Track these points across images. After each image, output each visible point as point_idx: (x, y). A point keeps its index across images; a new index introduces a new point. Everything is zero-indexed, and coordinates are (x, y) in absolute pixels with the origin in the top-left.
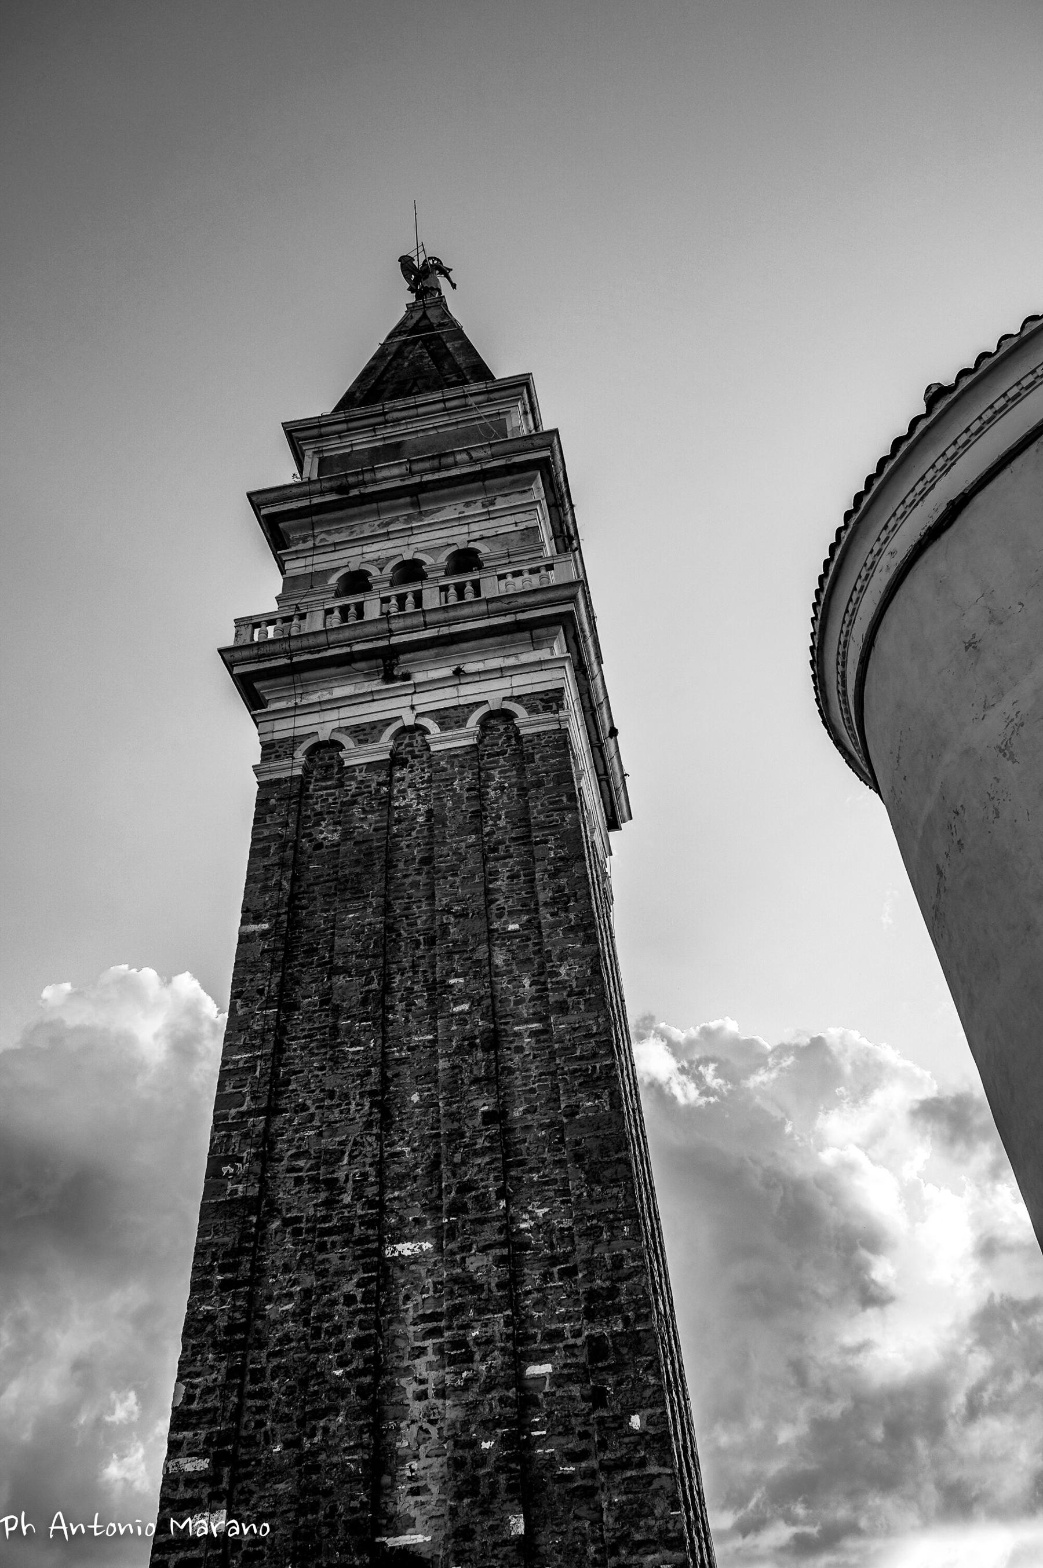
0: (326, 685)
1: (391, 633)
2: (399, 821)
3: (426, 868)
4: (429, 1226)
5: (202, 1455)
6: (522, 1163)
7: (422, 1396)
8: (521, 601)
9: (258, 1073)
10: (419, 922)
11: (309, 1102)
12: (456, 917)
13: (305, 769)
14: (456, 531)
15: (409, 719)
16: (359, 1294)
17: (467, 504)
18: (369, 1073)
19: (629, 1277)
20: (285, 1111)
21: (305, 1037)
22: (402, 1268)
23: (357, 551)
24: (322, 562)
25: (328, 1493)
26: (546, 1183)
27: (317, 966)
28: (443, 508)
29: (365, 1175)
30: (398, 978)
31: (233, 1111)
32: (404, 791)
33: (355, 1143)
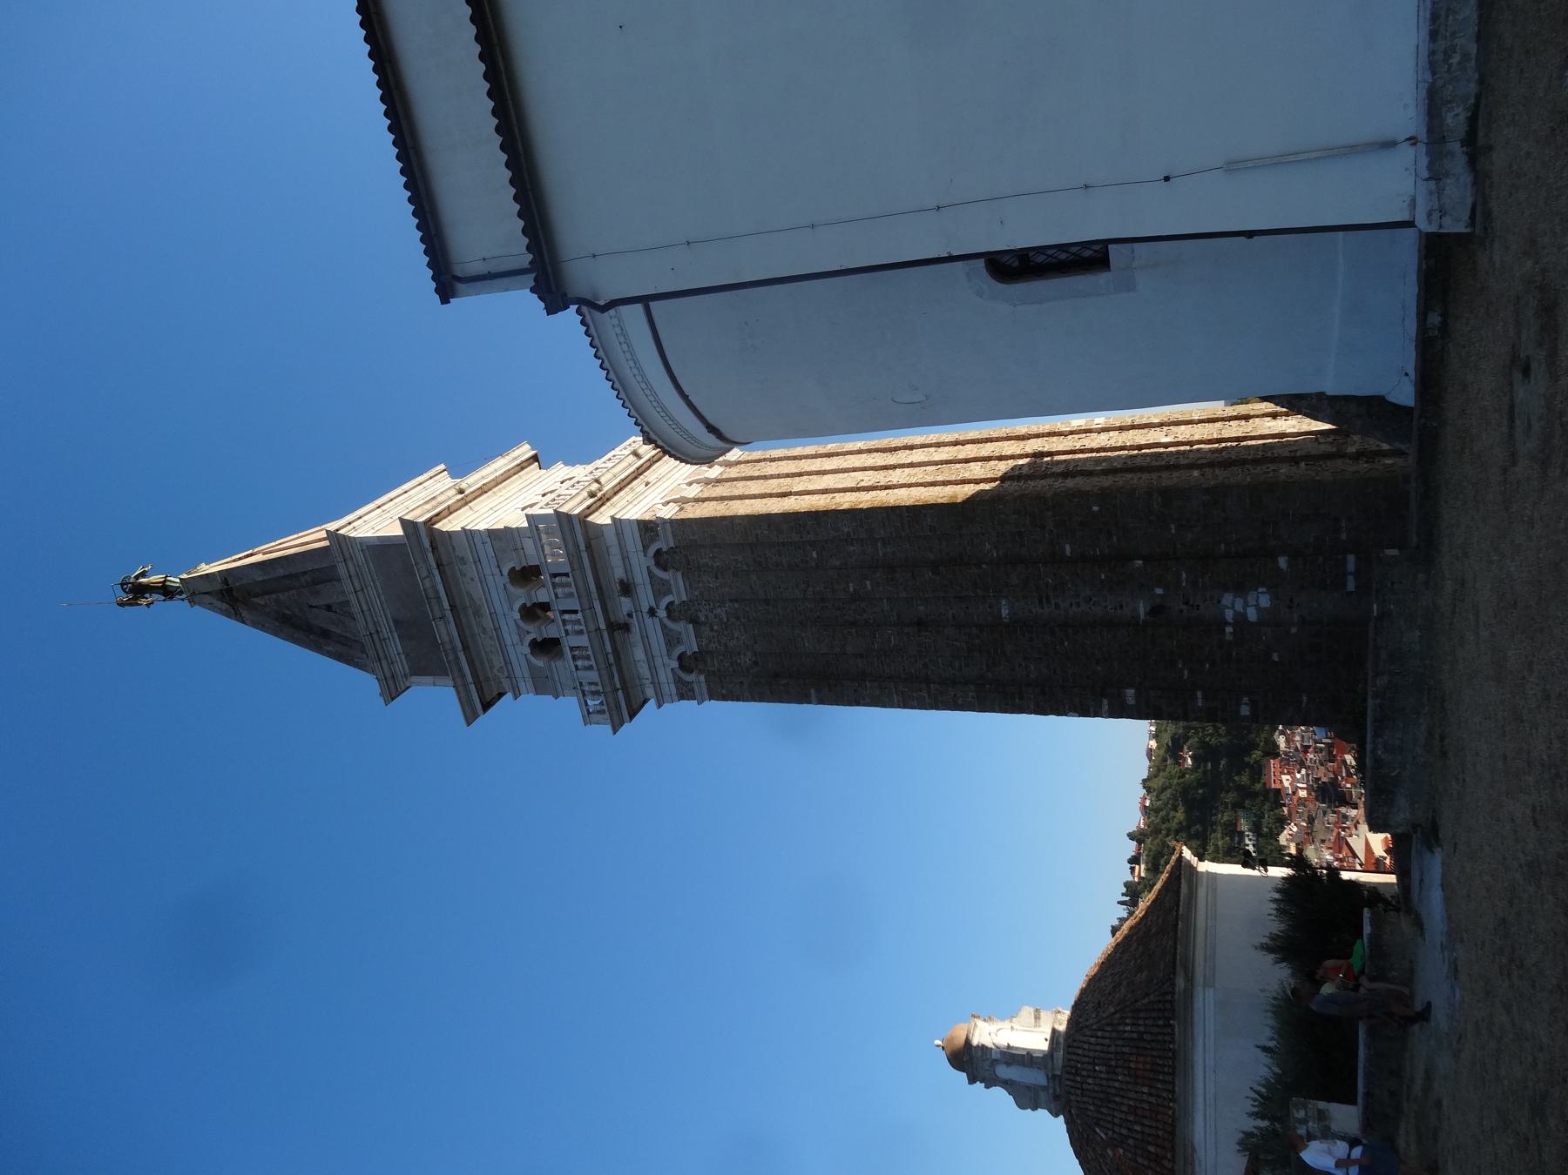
7: (1078, 604)
13: (701, 672)
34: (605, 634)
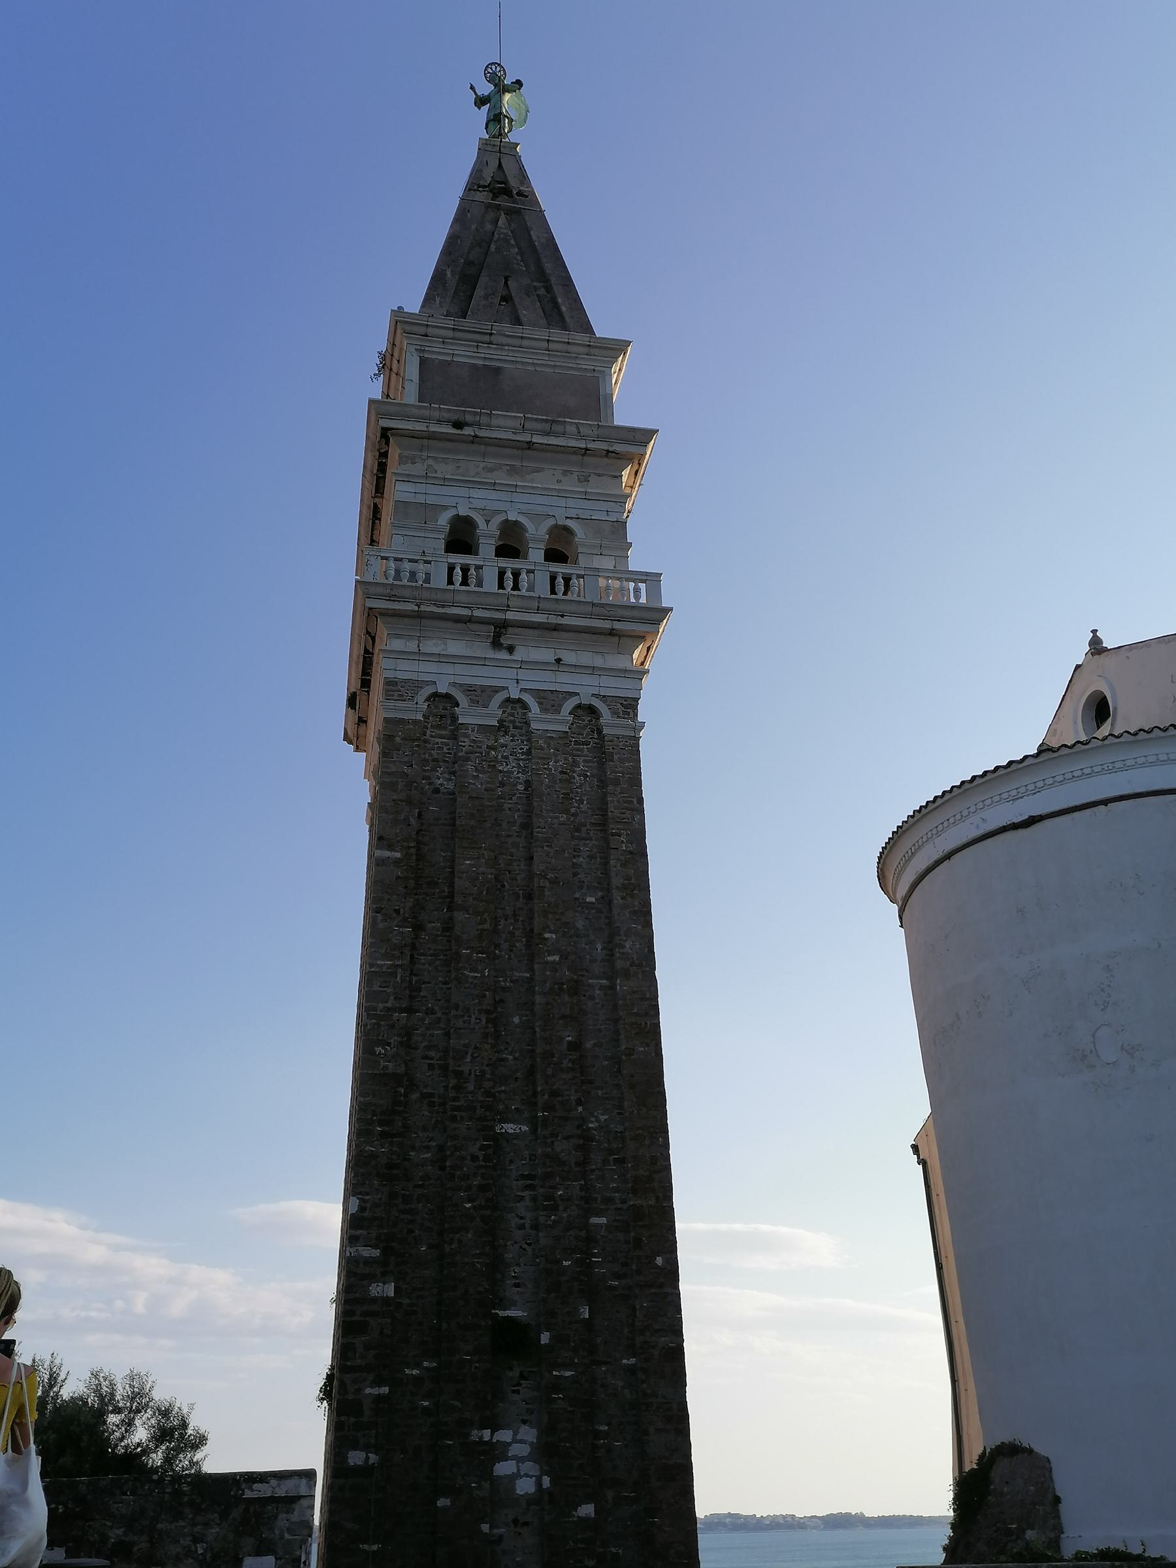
2: (502, 784)
3: (524, 832)
4: (526, 1115)
5: (375, 1247)
6: (591, 1082)
7: (522, 1227)
8: (620, 612)
10: (519, 878)
11: (436, 1008)
12: (551, 883)
16: (481, 1155)
18: (485, 996)
20: (418, 1011)
22: (508, 1141)
23: (463, 492)
24: (434, 494)
26: (607, 1099)
28: (543, 469)
29: (483, 1072)
30: (503, 922)
31: (381, 1006)
32: (506, 757)
33: (476, 1048)
34: (499, 615)
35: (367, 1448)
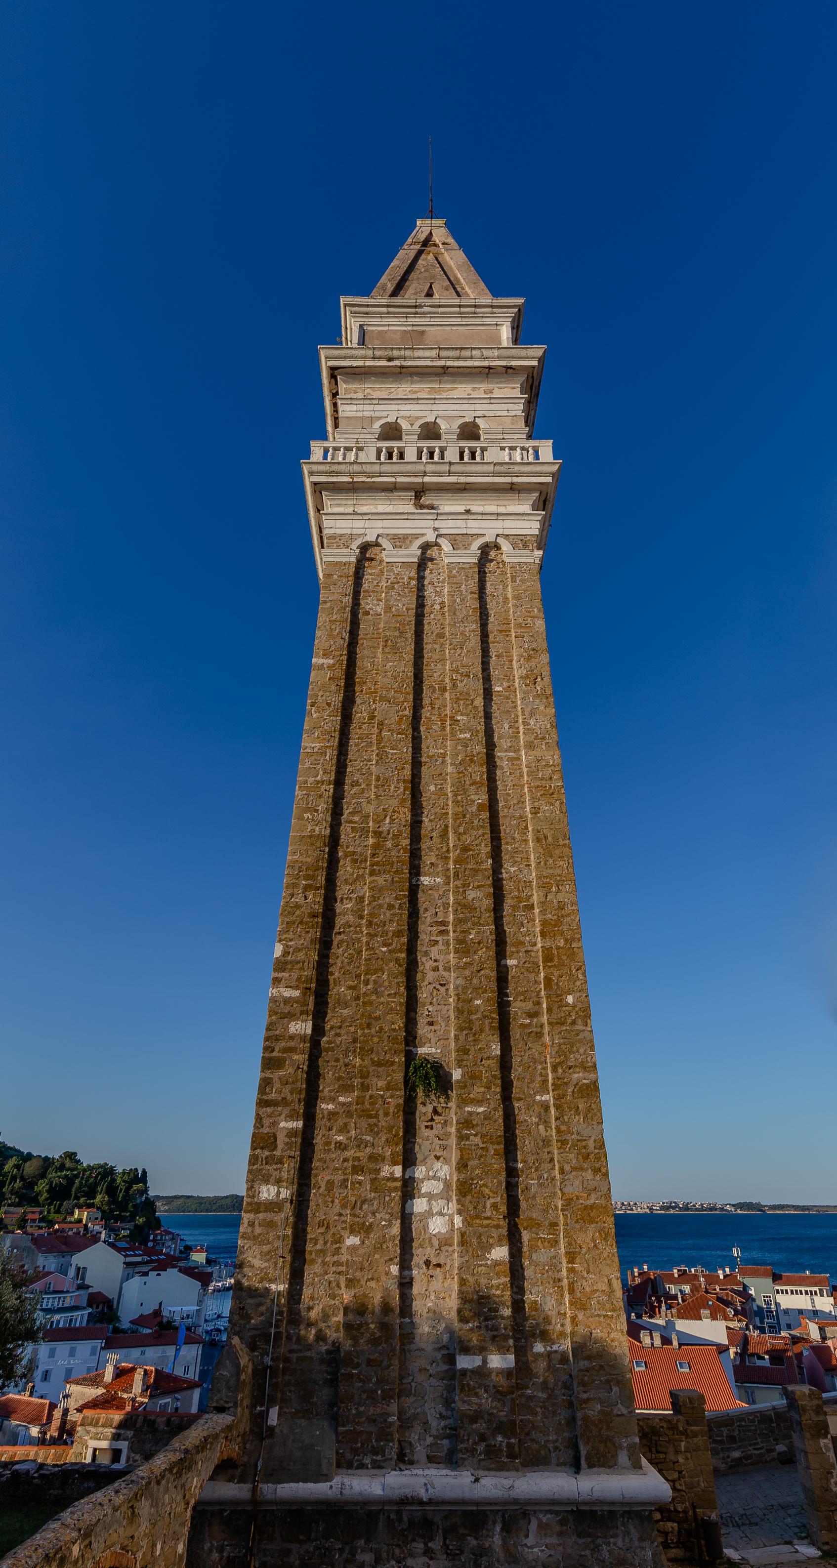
0: (372, 502)
1: (425, 474)
5: (296, 988)
7: (436, 969)
9: (327, 757)
14: (465, 407)
15: (431, 537)
17: (474, 389)
19: (569, 915)
21: (358, 738)
23: (395, 407)
25: (378, 1019)
27: (366, 694)
33: (394, 811)
35: (278, 1182)
